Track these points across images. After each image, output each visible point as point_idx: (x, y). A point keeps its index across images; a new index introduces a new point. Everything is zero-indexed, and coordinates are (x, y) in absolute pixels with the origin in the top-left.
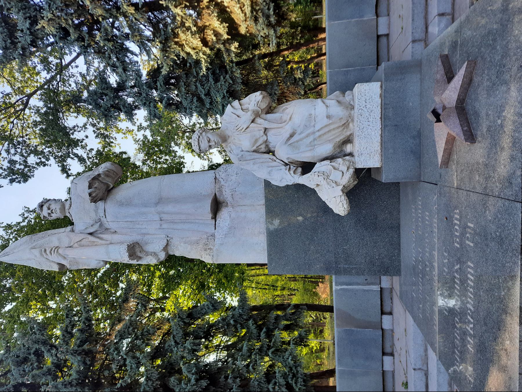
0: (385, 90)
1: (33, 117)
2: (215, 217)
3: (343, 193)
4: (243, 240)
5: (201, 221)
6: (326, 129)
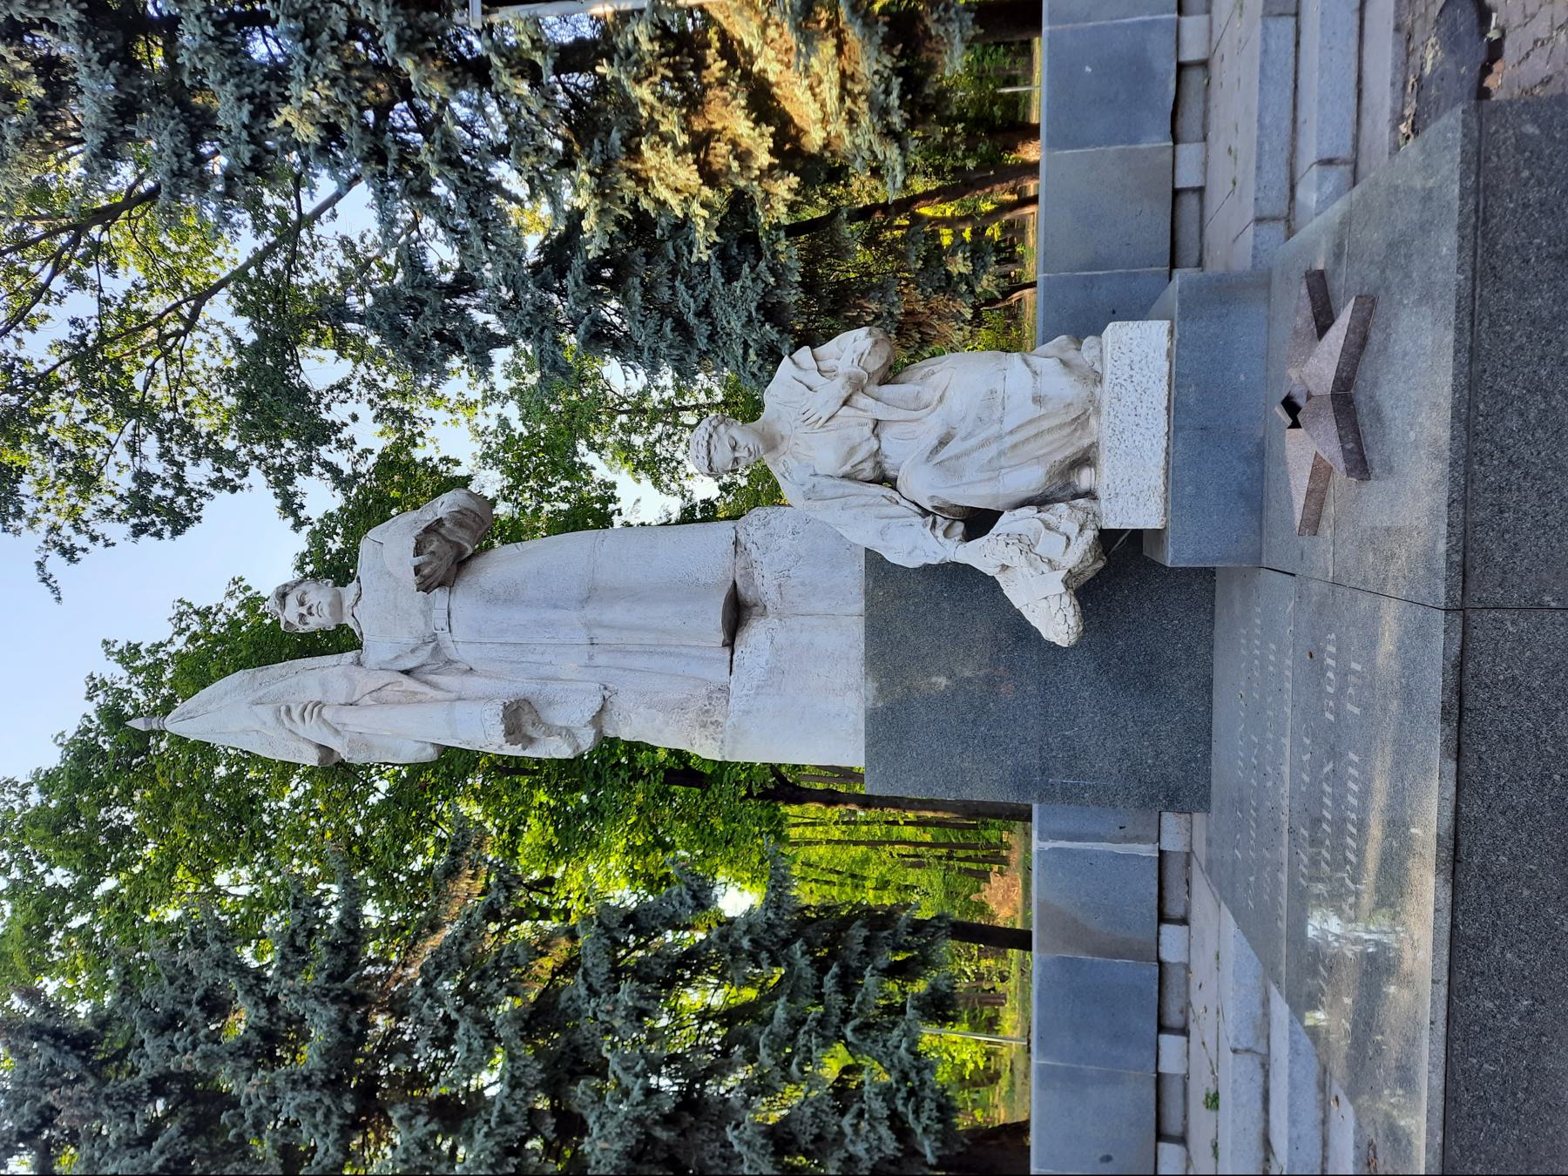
0: (1179, 341)
1: (202, 356)
2: (730, 643)
3: (1067, 588)
4: (805, 706)
5: (694, 652)
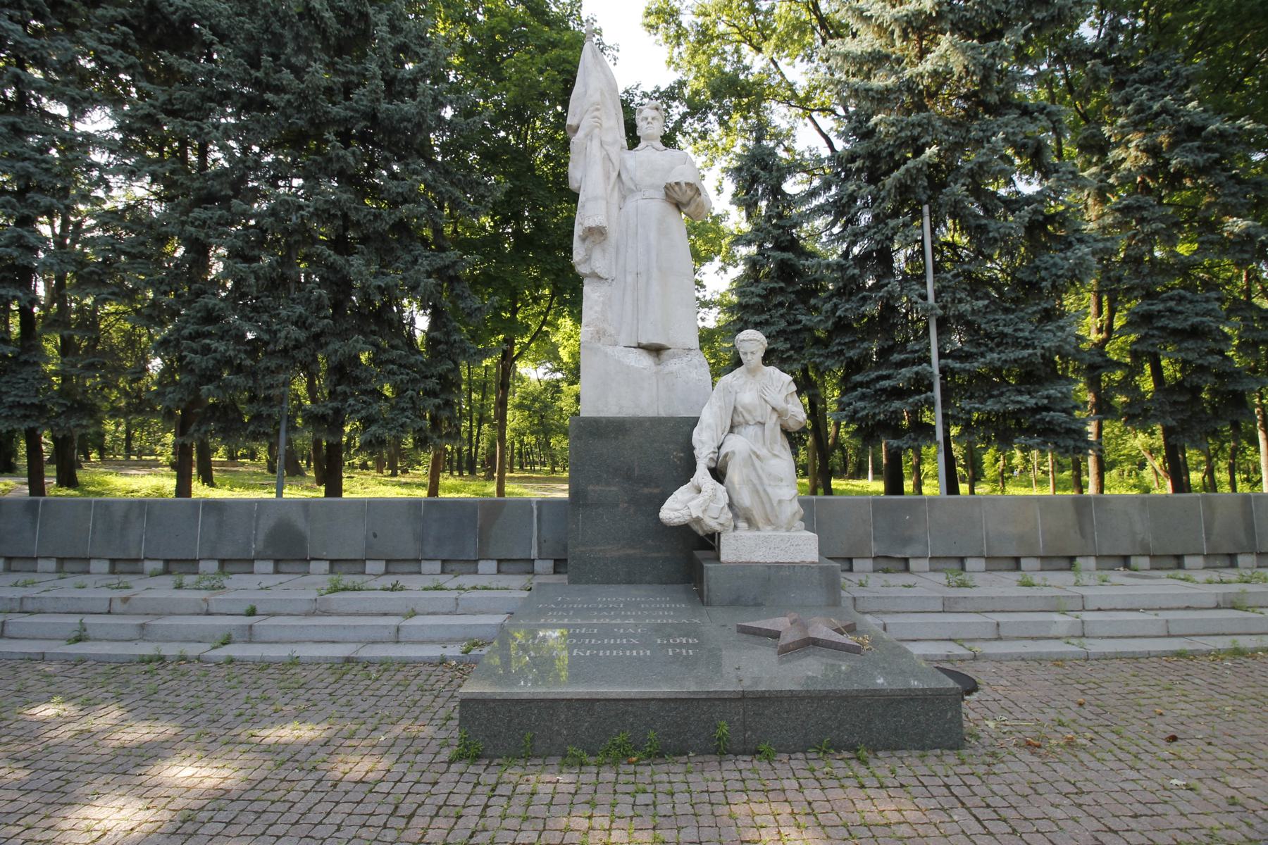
2: (640, 346)
6: (765, 499)
